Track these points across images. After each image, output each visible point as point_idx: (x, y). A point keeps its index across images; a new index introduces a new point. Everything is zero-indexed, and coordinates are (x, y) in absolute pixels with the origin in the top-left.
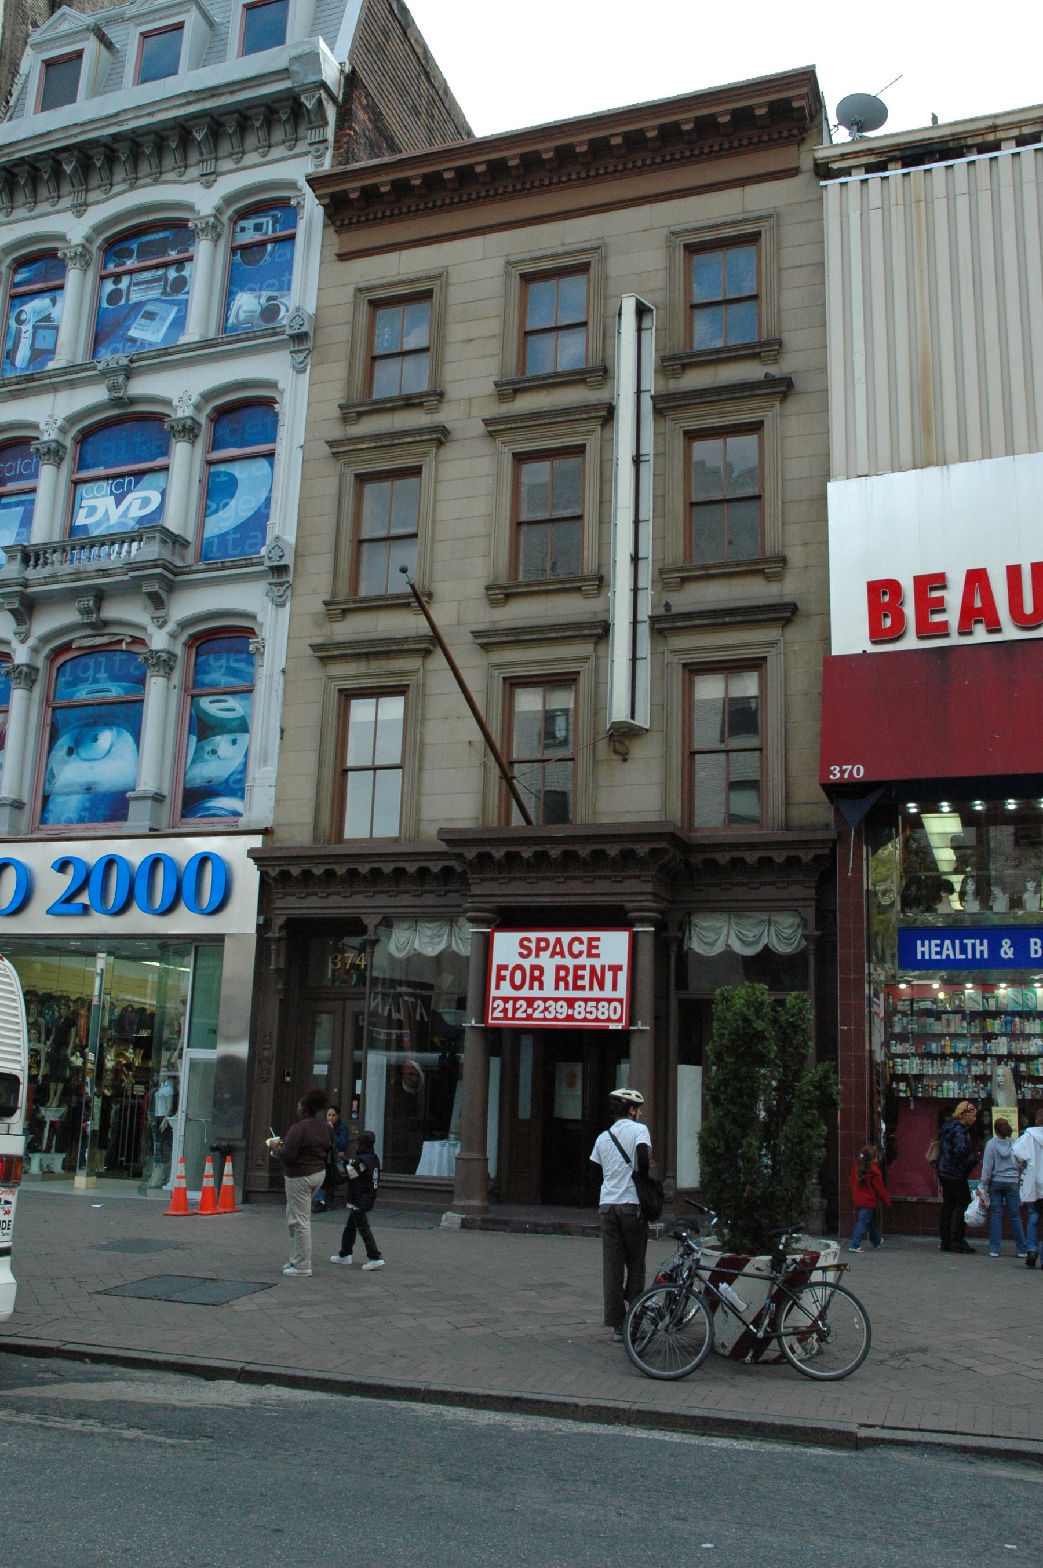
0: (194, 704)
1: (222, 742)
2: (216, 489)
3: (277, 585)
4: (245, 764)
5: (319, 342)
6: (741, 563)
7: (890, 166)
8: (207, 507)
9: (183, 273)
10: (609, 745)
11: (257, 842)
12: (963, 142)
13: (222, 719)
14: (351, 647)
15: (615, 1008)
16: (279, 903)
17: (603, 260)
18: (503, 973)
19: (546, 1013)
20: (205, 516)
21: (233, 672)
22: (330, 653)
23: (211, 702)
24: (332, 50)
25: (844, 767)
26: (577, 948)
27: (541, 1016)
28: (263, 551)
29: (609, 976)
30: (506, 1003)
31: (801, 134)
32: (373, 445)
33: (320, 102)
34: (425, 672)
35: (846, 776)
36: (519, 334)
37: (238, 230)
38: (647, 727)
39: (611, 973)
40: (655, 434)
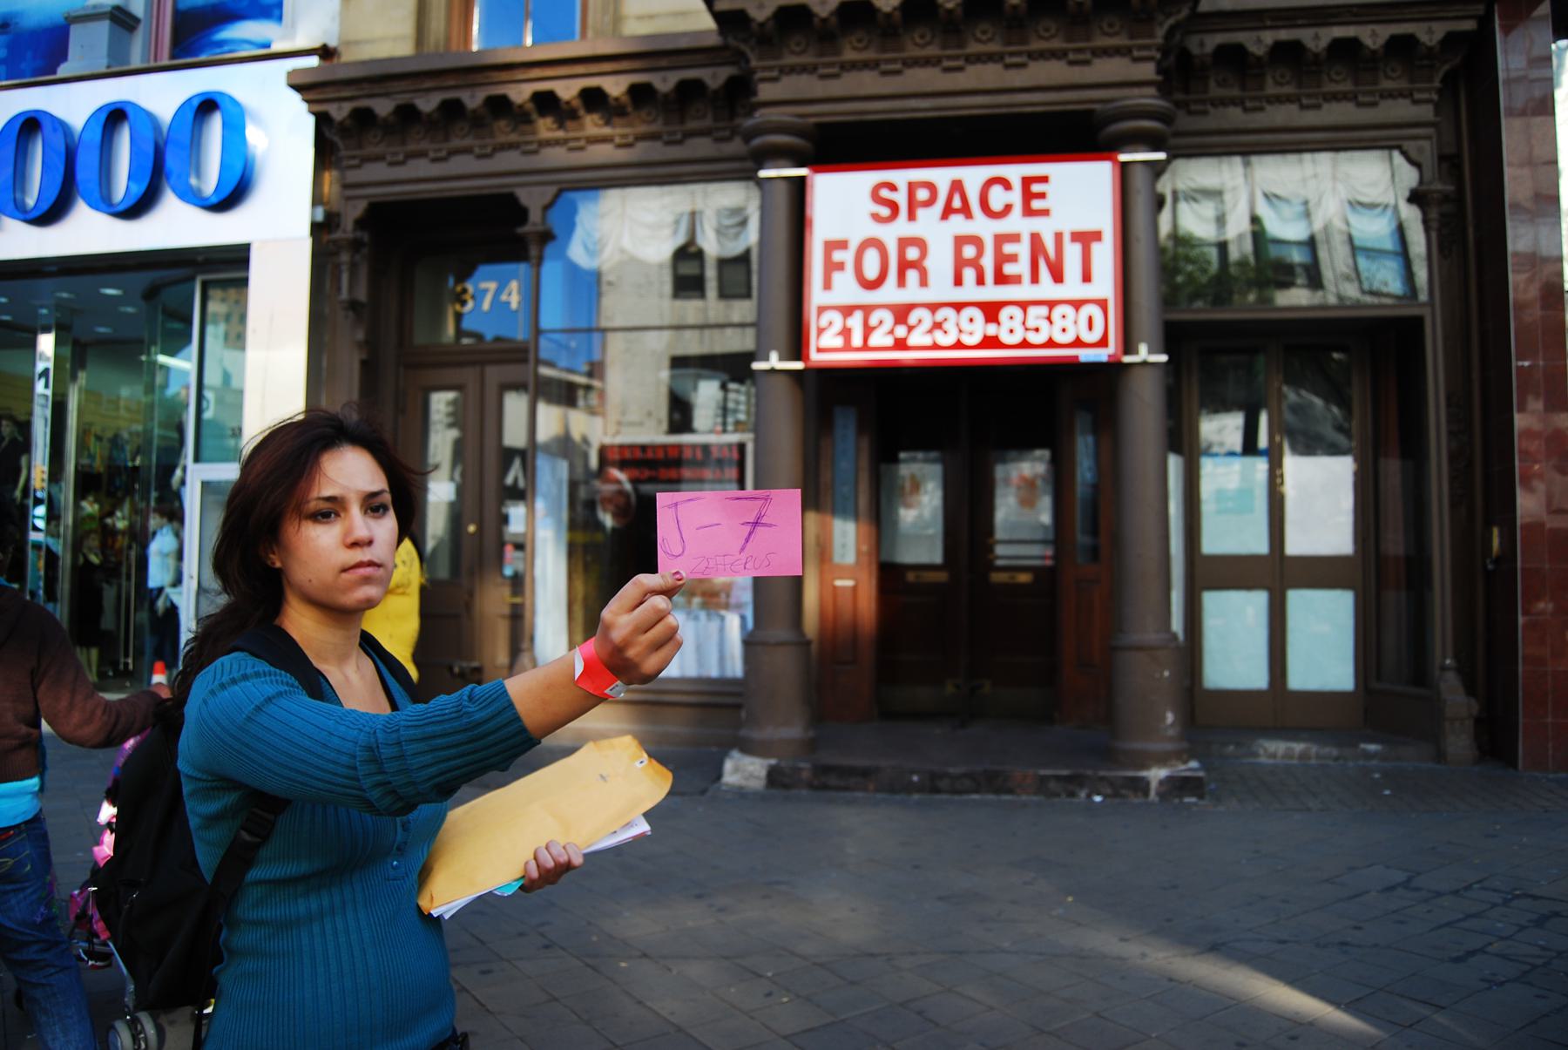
16: (354, 176)
18: (838, 256)
26: (998, 198)
27: (927, 341)
29: (1073, 253)
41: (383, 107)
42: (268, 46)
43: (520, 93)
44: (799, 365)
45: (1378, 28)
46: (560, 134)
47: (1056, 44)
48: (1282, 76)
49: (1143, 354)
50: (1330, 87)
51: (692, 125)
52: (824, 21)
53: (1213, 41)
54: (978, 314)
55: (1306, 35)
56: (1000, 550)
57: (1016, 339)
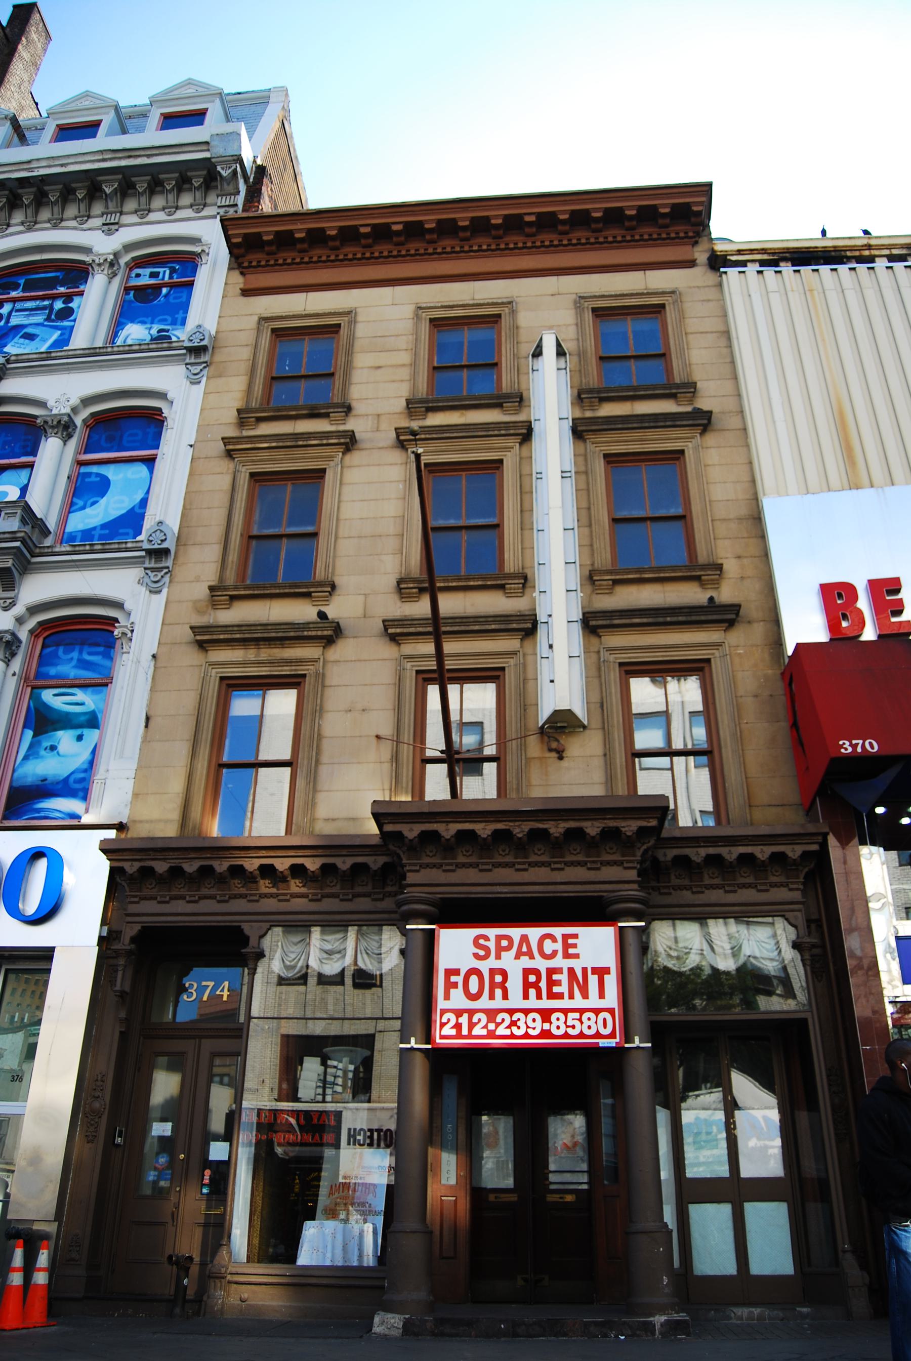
0: (35, 697)
1: (65, 739)
2: (84, 487)
3: (153, 569)
4: (91, 763)
5: (218, 358)
6: (670, 566)
7: (782, 264)
8: (72, 504)
9: (70, 305)
10: (542, 741)
11: (112, 834)
12: (843, 253)
13: (68, 714)
14: (240, 632)
15: (605, 1020)
16: (133, 908)
17: (513, 312)
18: (453, 979)
19: (514, 1029)
20: (69, 512)
21: (84, 664)
22: (215, 637)
23: (55, 695)
24: (250, 138)
25: (854, 742)
26: (549, 946)
27: (507, 1032)
28: (142, 537)
29: (593, 980)
30: (457, 1021)
31: (694, 237)
32: (274, 444)
33: (235, 172)
34: (325, 662)
35: (859, 750)
36: (428, 367)
37: (133, 275)
38: (586, 723)
39: (596, 977)
40: (575, 455)
41: (161, 867)
42: (79, 817)
43: (252, 864)
44: (429, 1046)
45: (765, 848)
46: (274, 890)
47: (580, 858)
48: (713, 874)
49: (637, 1042)
50: (742, 880)
51: (359, 889)
52: (448, 840)
53: (672, 853)
54: (537, 1016)
55: (724, 851)
56: (552, 1178)
57: (561, 1032)
